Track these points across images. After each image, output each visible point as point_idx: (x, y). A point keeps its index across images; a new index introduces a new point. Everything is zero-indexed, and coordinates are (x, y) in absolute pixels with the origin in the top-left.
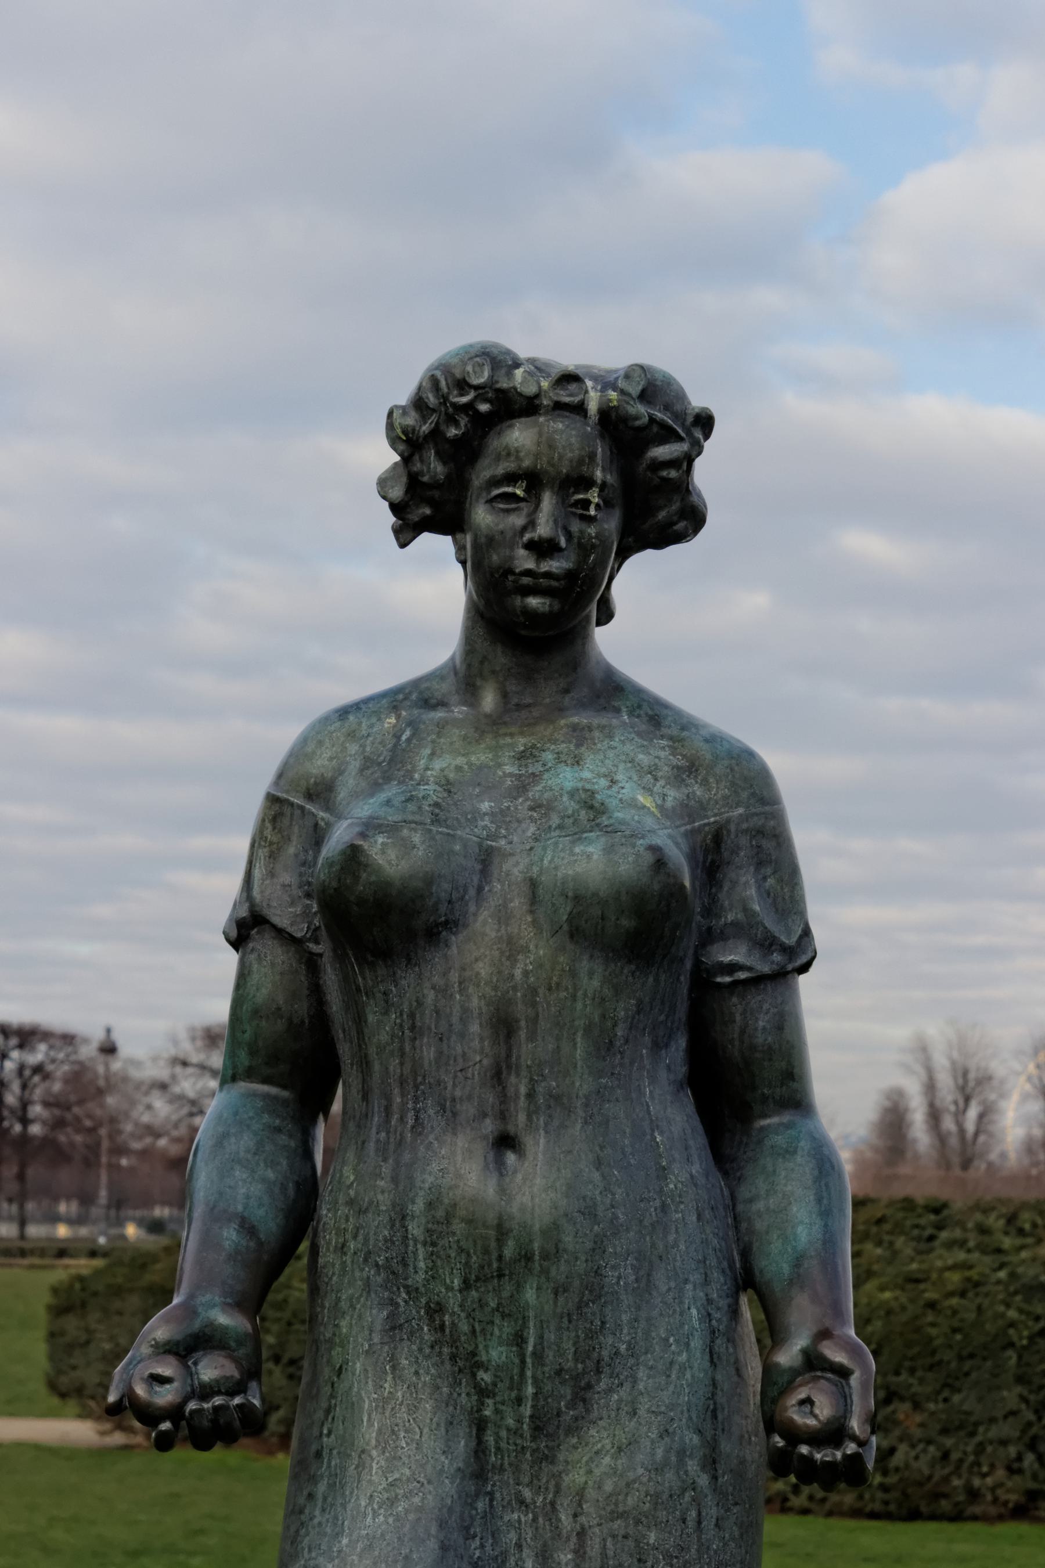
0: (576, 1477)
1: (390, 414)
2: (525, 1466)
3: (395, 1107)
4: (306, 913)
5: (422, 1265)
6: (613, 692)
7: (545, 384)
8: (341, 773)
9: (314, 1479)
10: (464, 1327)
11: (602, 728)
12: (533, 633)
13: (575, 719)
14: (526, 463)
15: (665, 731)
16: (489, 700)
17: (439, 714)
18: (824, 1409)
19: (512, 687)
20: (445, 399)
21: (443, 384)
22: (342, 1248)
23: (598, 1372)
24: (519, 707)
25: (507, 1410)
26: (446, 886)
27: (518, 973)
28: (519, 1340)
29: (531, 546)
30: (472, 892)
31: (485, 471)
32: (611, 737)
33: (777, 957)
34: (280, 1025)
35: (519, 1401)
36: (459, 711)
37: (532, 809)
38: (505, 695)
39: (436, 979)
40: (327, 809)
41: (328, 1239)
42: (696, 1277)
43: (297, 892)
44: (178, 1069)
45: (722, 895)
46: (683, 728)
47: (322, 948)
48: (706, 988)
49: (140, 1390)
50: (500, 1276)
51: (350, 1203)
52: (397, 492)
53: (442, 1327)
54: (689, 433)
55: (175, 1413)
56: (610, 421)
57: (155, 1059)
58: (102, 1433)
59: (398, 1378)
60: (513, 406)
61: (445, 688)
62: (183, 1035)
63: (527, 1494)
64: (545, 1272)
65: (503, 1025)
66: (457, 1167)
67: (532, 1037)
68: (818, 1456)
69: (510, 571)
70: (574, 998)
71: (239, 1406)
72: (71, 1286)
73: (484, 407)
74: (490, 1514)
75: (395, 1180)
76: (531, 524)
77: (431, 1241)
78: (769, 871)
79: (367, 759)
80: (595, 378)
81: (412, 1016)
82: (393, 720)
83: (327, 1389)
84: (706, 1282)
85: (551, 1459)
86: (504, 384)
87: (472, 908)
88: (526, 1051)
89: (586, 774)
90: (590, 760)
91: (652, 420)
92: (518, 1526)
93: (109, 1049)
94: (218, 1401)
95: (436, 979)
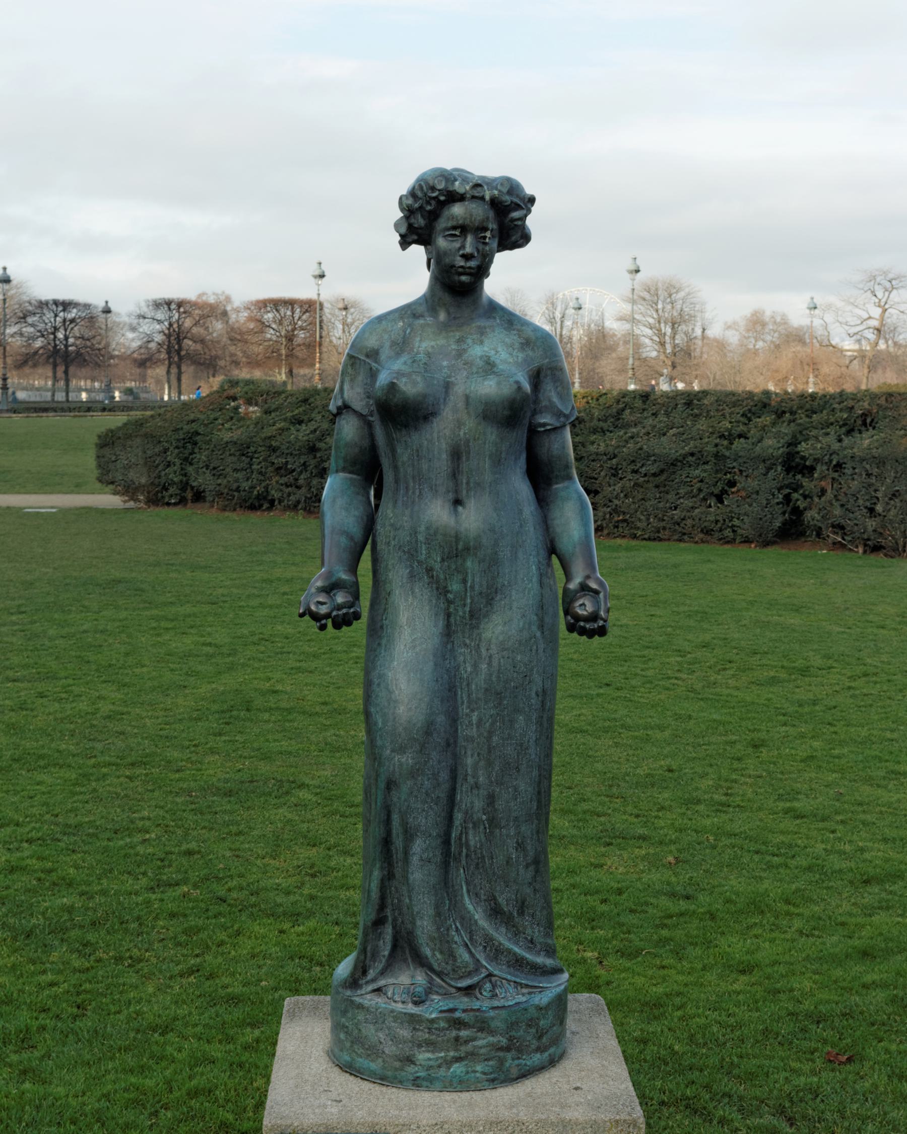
0: (487, 635)
1: (401, 198)
2: (467, 631)
3: (411, 487)
4: (367, 405)
5: (424, 552)
6: (493, 308)
7: (468, 188)
8: (382, 347)
9: (380, 637)
10: (442, 577)
12: (458, 287)
13: (478, 324)
14: (460, 222)
15: (515, 327)
16: (442, 316)
17: (421, 321)
18: (590, 608)
19: (452, 310)
20: (426, 195)
21: (425, 188)
22: (388, 544)
23: (496, 593)
24: (455, 318)
25: (460, 609)
26: (431, 399)
27: (462, 433)
28: (464, 581)
29: (463, 256)
30: (442, 400)
31: (442, 223)
32: (494, 331)
33: (562, 419)
34: (357, 450)
35: (465, 605)
36: (429, 320)
37: (464, 364)
38: (449, 313)
39: (428, 436)
40: (376, 362)
42: (534, 553)
43: (363, 396)
44: (141, 320)
45: (540, 395)
46: (522, 325)
47: (375, 419)
48: (533, 433)
49: (313, 608)
50: (457, 556)
52: (403, 230)
53: (433, 577)
54: (526, 206)
55: (327, 616)
56: (495, 203)
57: (129, 315)
58: (125, 502)
59: (414, 597)
60: (453, 197)
61: (421, 309)
62: (143, 304)
63: (468, 641)
64: (475, 554)
65: (456, 455)
66: (437, 512)
67: (468, 459)
68: (587, 626)
69: (453, 266)
70: (485, 443)
71: (354, 612)
72: (107, 434)
73: (442, 198)
74: (452, 650)
75: (411, 517)
76: (463, 247)
78: (559, 384)
79: (393, 342)
80: (488, 184)
81: (417, 451)
82: (401, 324)
83: (384, 601)
84: (538, 554)
85: (478, 628)
86: (451, 189)
87: (442, 407)
89: (486, 349)
90: (486, 342)
91: (512, 202)
93: (107, 311)
94: (344, 611)
95: (428, 436)
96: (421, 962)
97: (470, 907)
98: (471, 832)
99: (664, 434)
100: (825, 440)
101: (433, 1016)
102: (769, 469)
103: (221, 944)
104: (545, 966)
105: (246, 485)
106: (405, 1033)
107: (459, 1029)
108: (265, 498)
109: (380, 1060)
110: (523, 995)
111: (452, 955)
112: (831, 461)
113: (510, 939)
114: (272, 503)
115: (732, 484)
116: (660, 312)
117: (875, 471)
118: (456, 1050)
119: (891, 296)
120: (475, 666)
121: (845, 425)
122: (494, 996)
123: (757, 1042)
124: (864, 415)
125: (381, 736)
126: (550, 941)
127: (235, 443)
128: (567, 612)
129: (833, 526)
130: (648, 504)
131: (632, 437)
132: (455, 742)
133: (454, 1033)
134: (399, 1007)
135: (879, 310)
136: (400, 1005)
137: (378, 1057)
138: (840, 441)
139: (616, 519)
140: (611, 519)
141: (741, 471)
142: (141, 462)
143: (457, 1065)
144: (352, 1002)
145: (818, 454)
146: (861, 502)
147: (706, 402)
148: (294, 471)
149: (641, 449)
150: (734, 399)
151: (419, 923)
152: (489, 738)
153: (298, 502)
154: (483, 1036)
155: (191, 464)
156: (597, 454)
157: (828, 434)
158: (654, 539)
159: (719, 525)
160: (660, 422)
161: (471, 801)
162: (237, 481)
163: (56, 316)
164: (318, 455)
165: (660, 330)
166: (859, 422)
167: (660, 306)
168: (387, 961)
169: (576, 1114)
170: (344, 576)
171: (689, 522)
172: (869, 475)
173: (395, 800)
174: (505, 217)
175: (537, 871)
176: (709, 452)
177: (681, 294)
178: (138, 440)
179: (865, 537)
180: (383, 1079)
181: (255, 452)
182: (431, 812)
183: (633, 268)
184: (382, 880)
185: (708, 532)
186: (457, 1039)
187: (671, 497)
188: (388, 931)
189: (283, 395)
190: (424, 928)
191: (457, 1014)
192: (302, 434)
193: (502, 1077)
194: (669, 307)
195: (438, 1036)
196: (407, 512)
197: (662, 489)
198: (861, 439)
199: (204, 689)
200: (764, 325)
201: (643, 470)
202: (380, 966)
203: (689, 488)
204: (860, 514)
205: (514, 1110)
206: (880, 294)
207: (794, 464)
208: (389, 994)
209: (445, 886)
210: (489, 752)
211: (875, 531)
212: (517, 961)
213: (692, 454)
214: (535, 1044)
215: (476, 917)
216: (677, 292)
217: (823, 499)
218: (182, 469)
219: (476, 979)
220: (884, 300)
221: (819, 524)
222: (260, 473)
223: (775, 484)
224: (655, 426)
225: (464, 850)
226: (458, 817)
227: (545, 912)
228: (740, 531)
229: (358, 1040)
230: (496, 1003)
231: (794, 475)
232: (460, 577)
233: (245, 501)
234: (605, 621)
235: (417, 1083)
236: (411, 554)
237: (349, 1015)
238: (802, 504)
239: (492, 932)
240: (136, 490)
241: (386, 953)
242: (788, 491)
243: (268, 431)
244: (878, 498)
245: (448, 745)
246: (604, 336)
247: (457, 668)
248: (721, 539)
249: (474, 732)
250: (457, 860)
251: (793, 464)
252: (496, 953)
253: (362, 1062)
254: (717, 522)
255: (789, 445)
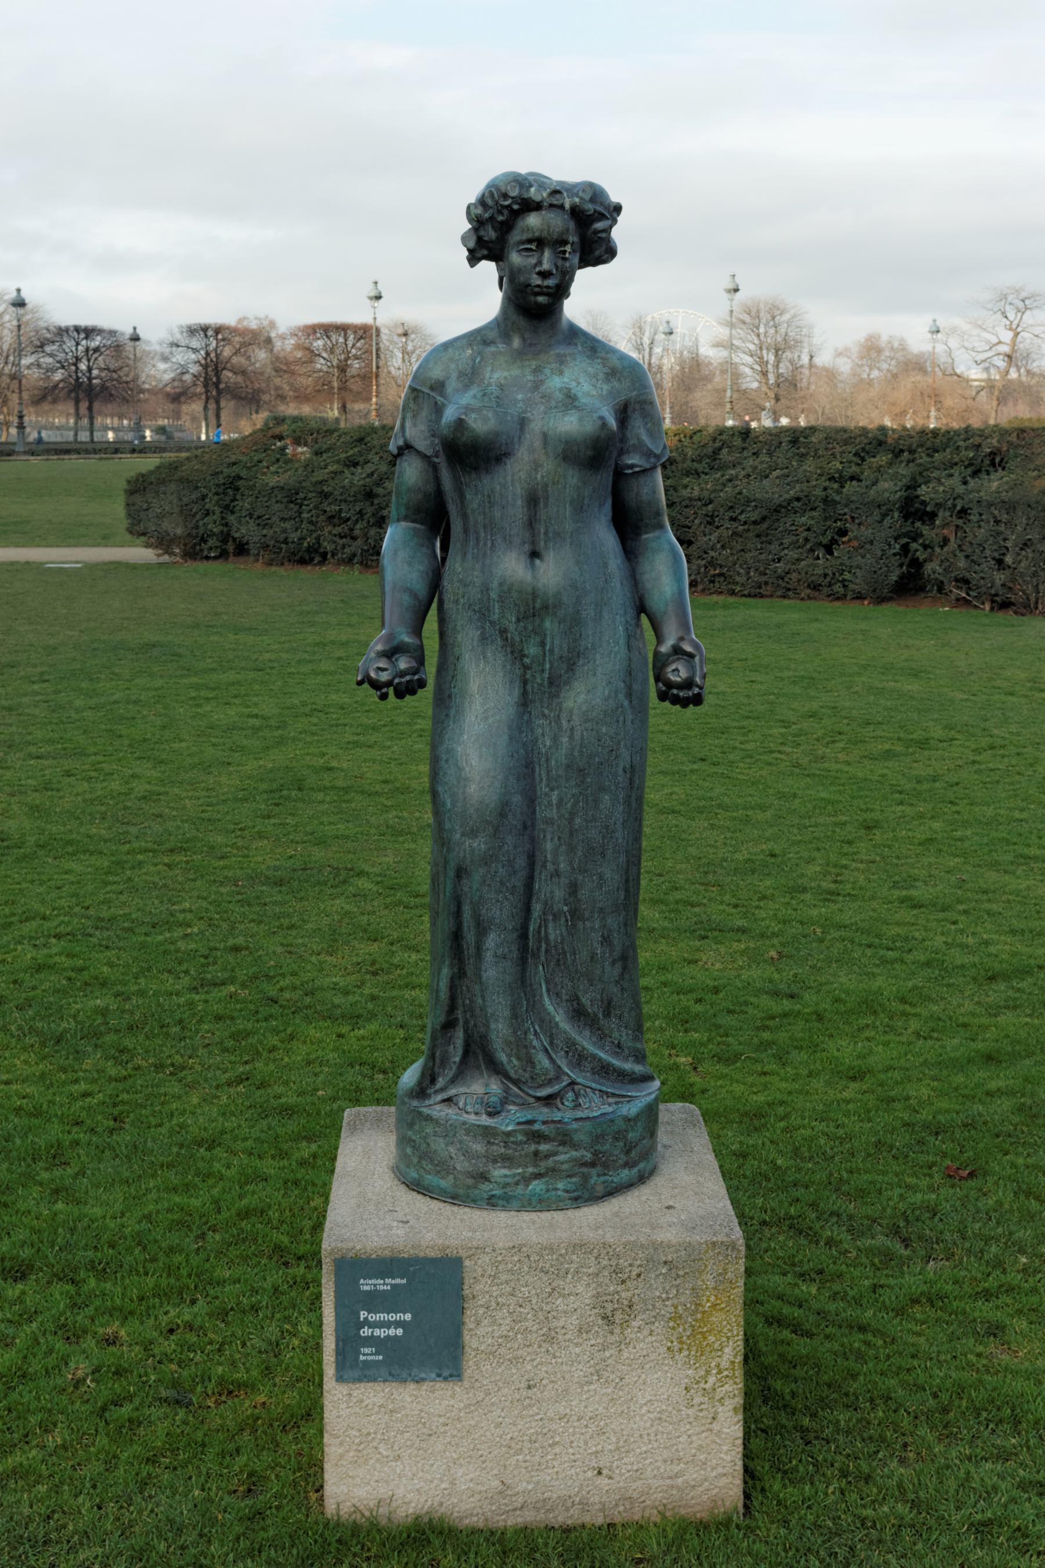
0: (569, 704)
1: (468, 207)
4: (432, 444)
6: (574, 333)
7: (545, 195)
10: (517, 639)
11: (570, 355)
12: (534, 308)
16: (516, 342)
17: (492, 349)
18: (684, 674)
19: (527, 336)
20: (497, 203)
22: (457, 602)
25: (538, 675)
27: (539, 476)
28: (543, 644)
29: (540, 273)
31: (515, 236)
33: (652, 460)
34: (420, 496)
35: (543, 671)
36: (502, 347)
38: (524, 339)
40: (442, 395)
41: (448, 597)
42: (621, 612)
43: (427, 434)
45: (628, 433)
47: (441, 461)
49: (373, 675)
51: (460, 581)
52: (472, 244)
55: (389, 684)
56: (577, 214)
58: (159, 555)
60: (529, 206)
61: (492, 335)
62: (176, 330)
63: (546, 712)
66: (512, 566)
67: (546, 506)
72: (137, 480)
73: (516, 207)
74: (529, 721)
75: (482, 571)
76: (540, 263)
77: (501, 600)
80: (567, 190)
86: (526, 196)
88: (542, 514)
89: (566, 380)
90: (567, 373)
92: (542, 726)
93: (135, 338)
94: (408, 678)
96: (495, 1068)
97: (551, 1008)
98: (551, 925)
99: (767, 477)
100: (949, 482)
101: (510, 1128)
102: (884, 516)
103: (273, 1049)
104: (634, 1073)
105: (294, 536)
106: (478, 1147)
107: (538, 1143)
108: (316, 551)
109: (451, 1177)
110: (610, 1105)
111: (531, 1062)
112: (955, 506)
113: (594, 1044)
114: (324, 556)
115: (843, 532)
116: (762, 337)
117: (1005, 517)
118: (536, 1166)
119: (1025, 317)
120: (555, 739)
121: (971, 465)
122: (577, 1106)
123: (869, 1155)
124: (993, 454)
125: (450, 819)
126: (639, 1045)
127: (282, 488)
128: (657, 679)
129: (957, 580)
130: (748, 555)
131: (730, 480)
132: (533, 825)
133: (533, 1147)
134: (472, 1118)
135: (1011, 334)
136: (473, 1117)
137: (448, 1173)
138: (965, 483)
139: (712, 572)
140: (706, 573)
141: (853, 518)
142: (176, 510)
143: (536, 1182)
144: (420, 1113)
145: (940, 498)
146: (988, 553)
147: (813, 439)
148: (348, 519)
149: (740, 493)
150: (845, 436)
151: (493, 1026)
152: (571, 821)
153: (354, 555)
154: (566, 1150)
155: (233, 512)
156: (691, 499)
157: (951, 475)
158: (755, 596)
159: (828, 579)
160: (762, 462)
161: (551, 891)
162: (285, 531)
163: (78, 344)
164: (376, 501)
165: (761, 358)
166: (987, 462)
167: (762, 330)
168: (458, 1068)
169: (668, 1235)
170: (407, 639)
171: (794, 576)
172: (997, 522)
173: (466, 889)
174: (586, 228)
175: (625, 968)
176: (817, 497)
177: (786, 317)
178: (173, 486)
179: (993, 592)
180: (454, 1198)
181: (305, 499)
182: (506, 903)
183: (731, 286)
184: (452, 978)
185: (816, 587)
186: (536, 1153)
187: (774, 547)
188: (459, 1035)
189: (336, 434)
190: (499, 1031)
191: (537, 1127)
192: (357, 478)
193: (586, 1195)
194: (772, 331)
195: (515, 1150)
196: (478, 566)
197: (764, 539)
198: (989, 481)
199: (251, 766)
200: (879, 351)
201: (742, 517)
202: (450, 1073)
203: (795, 538)
204: (987, 566)
205: (600, 1232)
206: (1011, 316)
207: (914, 510)
208: (461, 1105)
209: (522, 984)
210: (571, 835)
211: (1003, 585)
212: (603, 1067)
213: (798, 499)
214: (623, 1158)
215: (557, 1019)
216: (781, 314)
217: (946, 549)
218: (223, 518)
219: (556, 1088)
220: (1016, 322)
221: (941, 578)
222: (311, 522)
223: (891, 532)
224: (756, 468)
225: (544, 946)
226: (537, 908)
227: (633, 1013)
228: (851, 586)
229: (426, 1155)
230: (580, 1114)
231: (913, 523)
232: (538, 639)
233: (294, 554)
234: (701, 688)
235: (491, 1203)
236: (483, 613)
237: (417, 1127)
238: (921, 555)
239: (574, 1034)
240: (172, 541)
241: (457, 1059)
242: (906, 540)
243: (320, 475)
244: (1007, 548)
245: (525, 827)
246: (698, 365)
247: (535, 741)
248: (829, 596)
249: (554, 813)
250: (536, 955)
251: (912, 510)
252: (580, 1059)
253: (430, 1179)
254: (826, 575)
255: (908, 488)
